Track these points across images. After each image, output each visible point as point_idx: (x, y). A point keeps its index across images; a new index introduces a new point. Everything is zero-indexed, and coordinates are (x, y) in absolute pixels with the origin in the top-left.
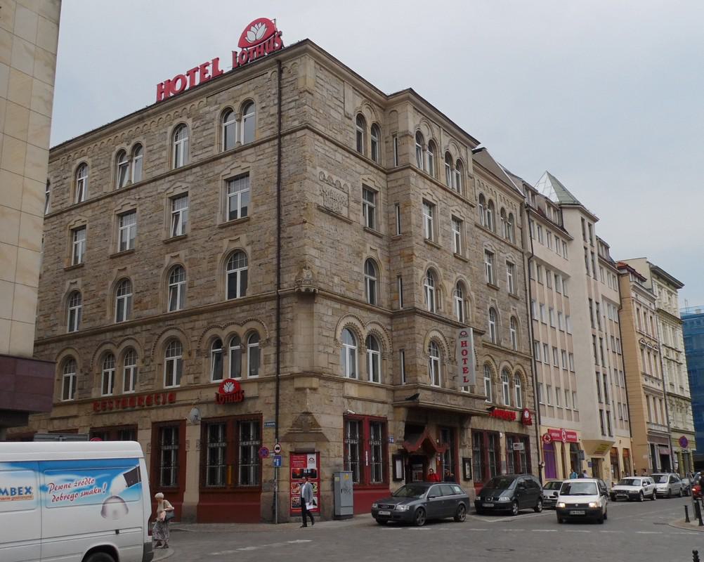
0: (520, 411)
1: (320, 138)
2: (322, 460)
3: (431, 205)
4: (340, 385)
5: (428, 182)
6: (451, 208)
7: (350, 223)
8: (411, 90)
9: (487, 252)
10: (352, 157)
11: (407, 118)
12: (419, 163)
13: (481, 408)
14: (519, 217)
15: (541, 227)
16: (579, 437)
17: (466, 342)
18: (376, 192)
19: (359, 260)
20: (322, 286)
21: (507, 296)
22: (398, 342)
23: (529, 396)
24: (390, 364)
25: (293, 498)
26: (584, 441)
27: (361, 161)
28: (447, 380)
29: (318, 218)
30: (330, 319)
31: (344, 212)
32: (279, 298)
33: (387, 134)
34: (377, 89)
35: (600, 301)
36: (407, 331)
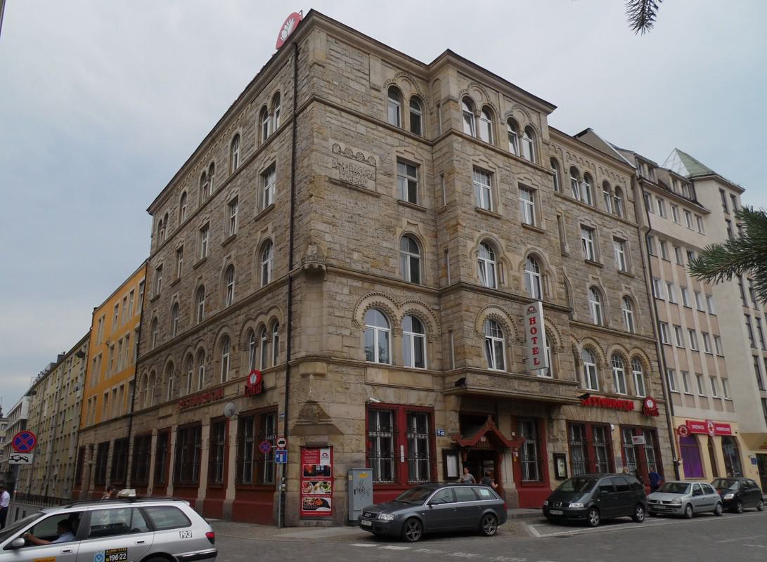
1: (334, 110)
2: (335, 455)
4: (362, 371)
5: (481, 148)
7: (377, 197)
8: (449, 52)
9: (584, 227)
10: (380, 128)
11: (448, 82)
12: (608, 209)
13: (570, 395)
15: (662, 200)
16: (735, 430)
17: (534, 318)
18: (419, 165)
19: (390, 235)
20: (334, 262)
21: (617, 274)
23: (655, 383)
25: (304, 499)
26: (742, 435)
28: (514, 363)
29: (328, 191)
31: (370, 185)
32: (291, 280)
33: (431, 106)
36: (455, 310)
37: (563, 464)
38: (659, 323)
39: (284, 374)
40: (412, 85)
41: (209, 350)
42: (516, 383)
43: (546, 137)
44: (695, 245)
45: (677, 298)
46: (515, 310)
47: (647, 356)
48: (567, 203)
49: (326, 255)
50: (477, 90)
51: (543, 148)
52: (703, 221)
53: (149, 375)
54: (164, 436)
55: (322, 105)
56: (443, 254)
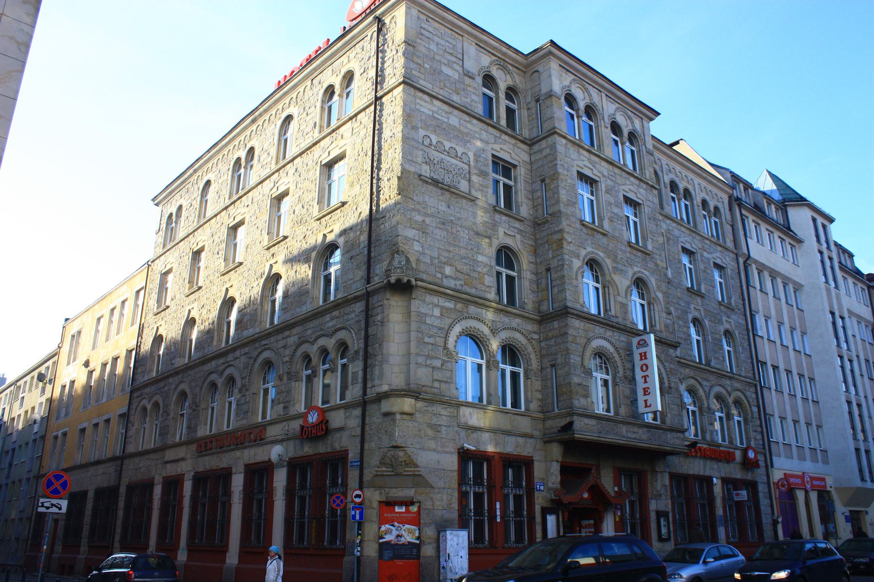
0: (743, 450)
3: (590, 182)
5: (585, 153)
6: (622, 187)
9: (685, 250)
10: (475, 121)
11: (550, 76)
14: (728, 213)
18: (515, 166)
22: (549, 355)
23: (756, 431)
24: (538, 385)
27: (490, 128)
28: (622, 406)
30: (437, 323)
31: (464, 186)
34: (510, 47)
35: (846, 315)
37: (666, 523)
38: (758, 361)
39: (358, 412)
40: (508, 75)
41: (243, 378)
42: (624, 429)
43: (650, 144)
44: (790, 276)
45: (774, 336)
46: (623, 343)
47: (748, 401)
48: (668, 221)
49: (414, 267)
50: (579, 87)
51: (647, 159)
52: (797, 251)
53: (149, 407)
54: (173, 484)
55: (412, 89)
56: (544, 273)
